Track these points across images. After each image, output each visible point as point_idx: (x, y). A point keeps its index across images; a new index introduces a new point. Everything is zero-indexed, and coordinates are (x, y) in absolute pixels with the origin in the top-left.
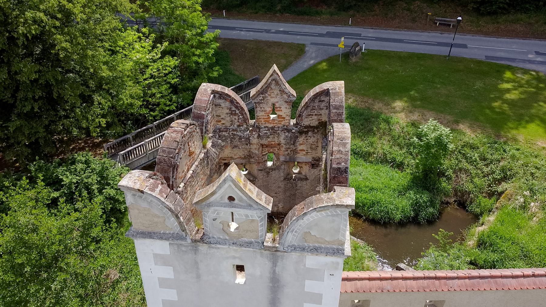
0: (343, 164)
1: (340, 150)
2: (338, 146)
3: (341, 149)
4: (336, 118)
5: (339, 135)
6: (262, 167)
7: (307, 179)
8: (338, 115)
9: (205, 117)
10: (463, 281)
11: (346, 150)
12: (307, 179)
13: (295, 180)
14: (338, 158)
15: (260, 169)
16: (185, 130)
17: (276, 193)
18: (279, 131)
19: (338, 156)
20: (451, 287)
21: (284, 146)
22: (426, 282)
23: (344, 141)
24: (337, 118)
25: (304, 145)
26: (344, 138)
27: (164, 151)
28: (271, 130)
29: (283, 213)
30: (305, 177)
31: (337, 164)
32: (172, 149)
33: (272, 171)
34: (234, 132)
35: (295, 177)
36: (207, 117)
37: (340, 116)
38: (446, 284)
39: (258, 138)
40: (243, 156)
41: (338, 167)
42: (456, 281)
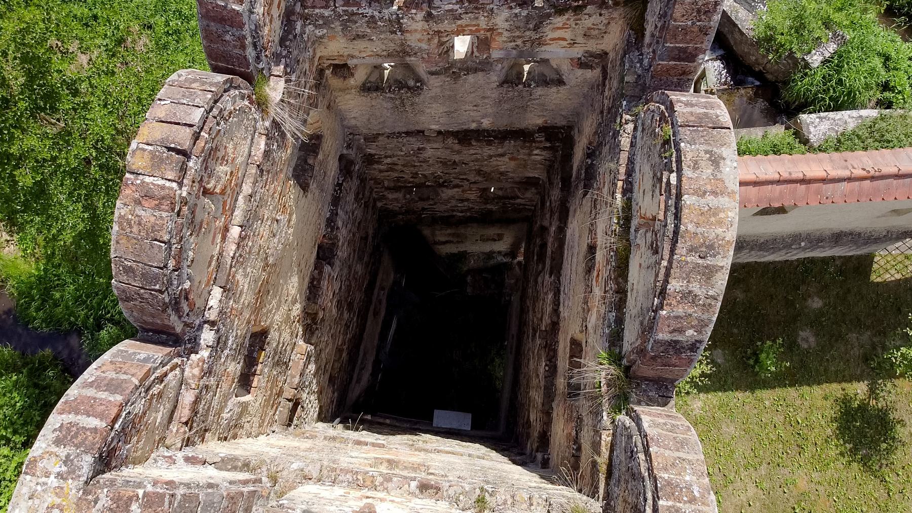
0: (690, 332)
1: (690, 292)
2: (688, 276)
3: (695, 287)
4: (690, 23)
5: (700, 230)
6: (441, 64)
7: (560, 82)
8: (699, 11)
9: (245, 19)
10: (857, 183)
11: (711, 293)
12: (560, 82)
13: (529, 86)
14: (677, 317)
15: (434, 69)
16: (181, 185)
17: (475, 106)
18: (491, 6)
19: (680, 311)
20: (827, 198)
21: (506, 34)
22: (778, 188)
23: (710, 261)
24: (693, 24)
25: (567, 30)
26: (711, 247)
27: (128, 270)
28: (466, 4)
29: (492, 131)
30: (555, 77)
31: (670, 333)
32: (152, 266)
33: (468, 74)
34: (350, 9)
35: (529, 73)
36: (253, 13)
37: (703, 17)
38: (818, 192)
39: (427, 21)
40: (385, 53)
41: (674, 339)
42: (843, 186)
